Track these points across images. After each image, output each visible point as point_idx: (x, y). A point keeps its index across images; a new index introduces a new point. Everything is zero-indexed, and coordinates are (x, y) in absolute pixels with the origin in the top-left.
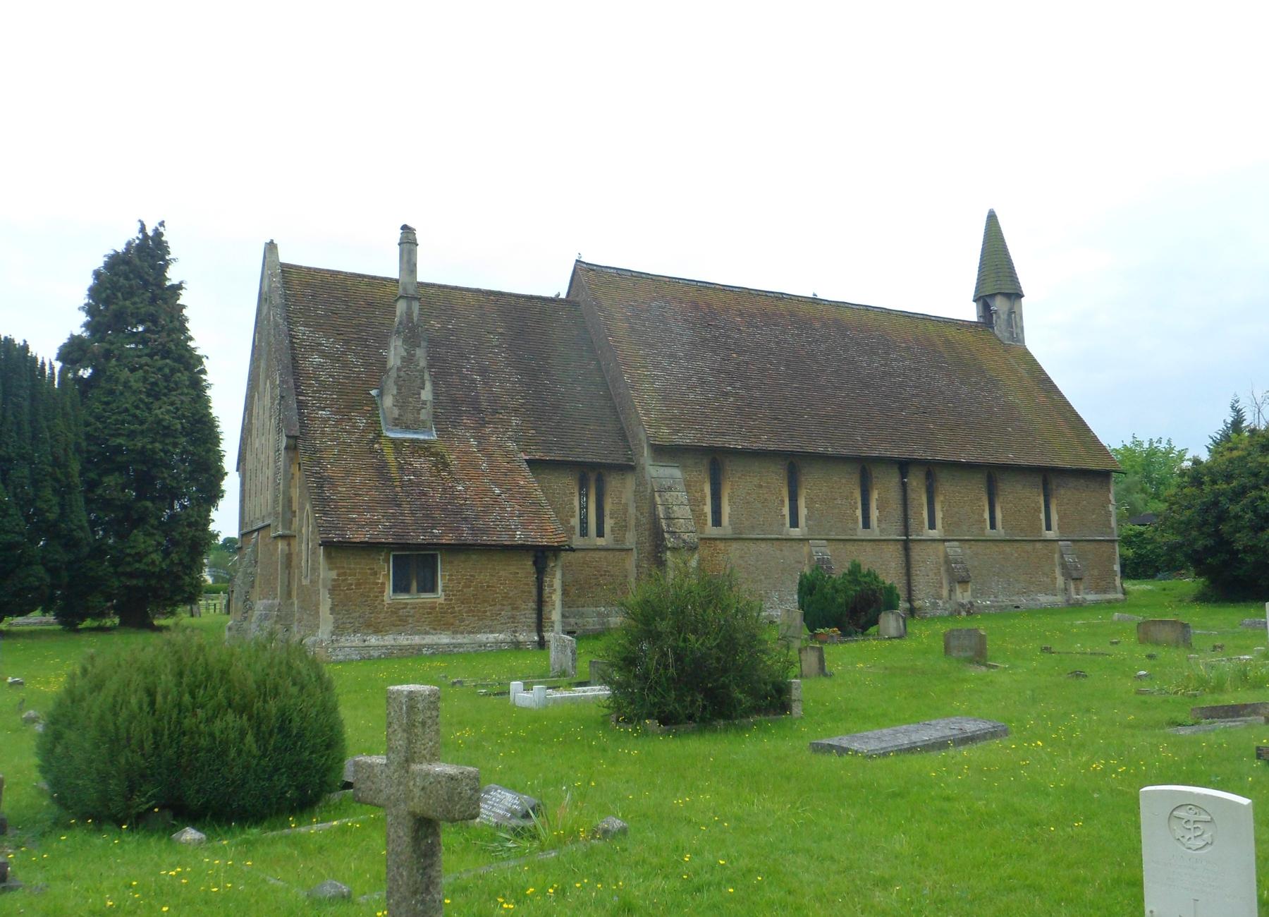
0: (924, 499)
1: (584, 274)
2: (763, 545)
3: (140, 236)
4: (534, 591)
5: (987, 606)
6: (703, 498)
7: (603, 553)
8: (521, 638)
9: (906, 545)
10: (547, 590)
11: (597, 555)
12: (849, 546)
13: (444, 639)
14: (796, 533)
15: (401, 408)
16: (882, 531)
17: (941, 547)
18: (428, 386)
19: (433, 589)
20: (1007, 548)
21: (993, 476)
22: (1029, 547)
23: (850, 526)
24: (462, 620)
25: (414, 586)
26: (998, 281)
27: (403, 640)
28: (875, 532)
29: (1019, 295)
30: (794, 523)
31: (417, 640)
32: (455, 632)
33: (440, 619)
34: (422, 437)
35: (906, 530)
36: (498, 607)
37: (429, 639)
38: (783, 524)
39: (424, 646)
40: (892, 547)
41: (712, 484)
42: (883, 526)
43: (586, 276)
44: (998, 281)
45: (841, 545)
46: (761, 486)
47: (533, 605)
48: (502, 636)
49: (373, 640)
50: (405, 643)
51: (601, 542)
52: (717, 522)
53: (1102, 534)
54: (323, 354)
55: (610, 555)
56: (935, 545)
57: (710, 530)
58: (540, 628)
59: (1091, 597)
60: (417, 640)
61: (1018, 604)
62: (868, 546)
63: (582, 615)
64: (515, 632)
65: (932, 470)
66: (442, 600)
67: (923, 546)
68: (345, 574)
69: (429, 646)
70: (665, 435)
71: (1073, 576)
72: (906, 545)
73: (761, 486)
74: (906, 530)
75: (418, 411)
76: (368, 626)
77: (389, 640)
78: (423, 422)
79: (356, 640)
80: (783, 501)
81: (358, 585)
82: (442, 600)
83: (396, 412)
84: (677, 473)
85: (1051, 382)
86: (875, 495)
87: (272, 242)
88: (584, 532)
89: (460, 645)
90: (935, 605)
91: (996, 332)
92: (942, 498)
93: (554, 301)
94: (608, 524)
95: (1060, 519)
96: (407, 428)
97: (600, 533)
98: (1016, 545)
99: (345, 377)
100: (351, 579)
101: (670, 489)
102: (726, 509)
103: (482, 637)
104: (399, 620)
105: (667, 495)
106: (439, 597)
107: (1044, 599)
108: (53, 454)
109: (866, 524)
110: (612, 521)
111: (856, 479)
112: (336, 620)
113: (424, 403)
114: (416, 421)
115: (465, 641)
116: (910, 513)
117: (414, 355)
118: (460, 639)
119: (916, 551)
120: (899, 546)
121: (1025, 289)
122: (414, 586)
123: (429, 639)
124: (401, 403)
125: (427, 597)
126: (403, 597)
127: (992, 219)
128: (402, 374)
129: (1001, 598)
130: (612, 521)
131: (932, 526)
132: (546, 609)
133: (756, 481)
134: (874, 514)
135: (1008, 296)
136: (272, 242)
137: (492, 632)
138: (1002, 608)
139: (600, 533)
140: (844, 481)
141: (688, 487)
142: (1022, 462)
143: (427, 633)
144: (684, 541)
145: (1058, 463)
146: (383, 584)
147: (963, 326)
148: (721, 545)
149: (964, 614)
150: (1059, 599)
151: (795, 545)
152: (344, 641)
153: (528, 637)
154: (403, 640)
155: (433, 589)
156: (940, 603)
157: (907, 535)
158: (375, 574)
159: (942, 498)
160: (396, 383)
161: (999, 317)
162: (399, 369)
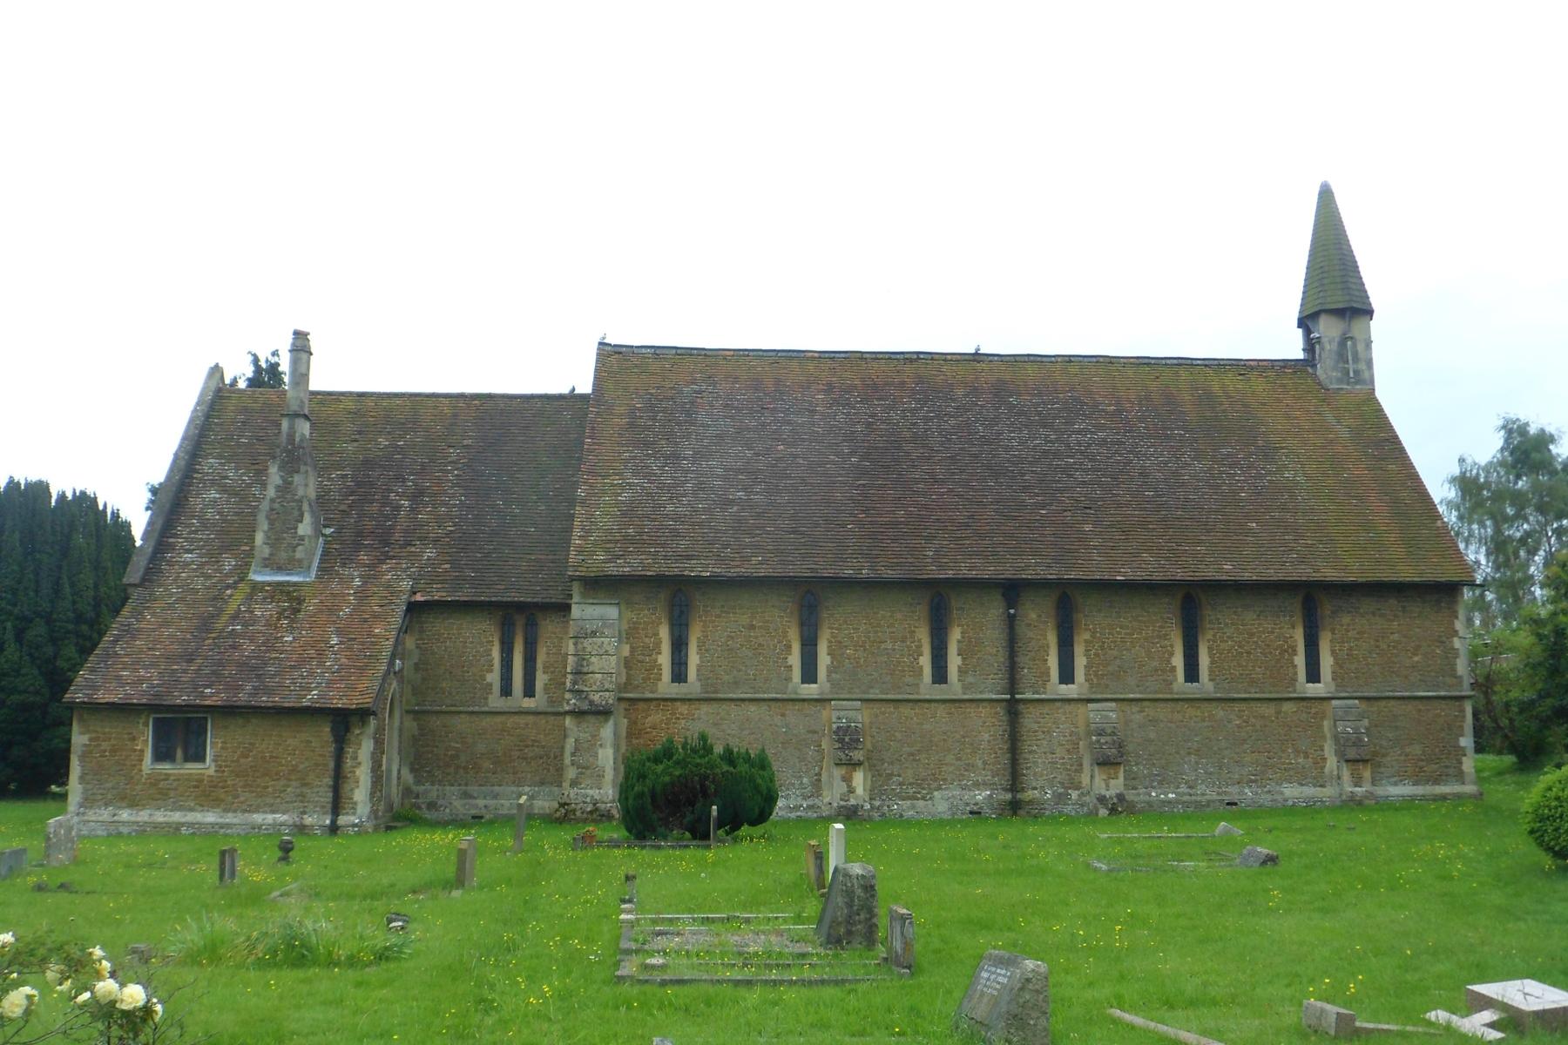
0: (1052, 639)
1: (612, 358)
2: (753, 708)
3: (252, 368)
4: (332, 765)
5: (1170, 802)
6: (658, 644)
7: (531, 718)
8: (308, 820)
9: (1013, 709)
10: (349, 762)
11: (522, 720)
12: (906, 710)
13: (210, 817)
14: (811, 690)
15: (272, 546)
16: (966, 688)
17: (1081, 709)
18: (307, 518)
19: (200, 758)
20: (1219, 712)
21: (1192, 601)
22: (1268, 710)
23: (908, 679)
24: (237, 797)
25: (179, 753)
26: (1336, 295)
27: (160, 817)
28: (955, 685)
29: (1368, 313)
30: (809, 675)
31: (177, 817)
32: (226, 810)
33: (207, 794)
34: (294, 579)
35: (1013, 684)
36: (282, 782)
37: (191, 817)
38: (789, 679)
39: (183, 824)
40: (984, 711)
41: (672, 626)
42: (970, 679)
43: (615, 361)
44: (1336, 295)
45: (891, 708)
46: (752, 627)
47: (328, 781)
48: (285, 817)
49: (125, 815)
50: (161, 820)
51: (529, 703)
52: (679, 675)
53: (1437, 687)
54: (224, 489)
55: (542, 720)
56: (1068, 707)
57: (666, 686)
58: (336, 808)
59: (1406, 790)
60: (177, 817)
61: (1235, 799)
62: (941, 710)
63: (495, 797)
64: (304, 813)
65: (1067, 600)
66: (211, 772)
67: (1046, 709)
68: (97, 739)
69: (190, 825)
70: (600, 562)
71: (1358, 758)
72: (1013, 709)
73: (752, 627)
74: (1013, 684)
75: (294, 548)
76: (123, 799)
77: (144, 816)
78: (300, 561)
79: (105, 814)
80: (789, 647)
81: (114, 751)
82: (211, 772)
83: (267, 551)
84: (612, 612)
85: (1399, 443)
86: (955, 635)
87: (217, 365)
88: (506, 691)
89: (228, 826)
90: (1061, 798)
91: (1319, 372)
92: (1087, 636)
93: (572, 398)
94: (541, 679)
95: (1338, 663)
96: (280, 569)
97: (529, 691)
98: (1237, 706)
99: (237, 514)
100: (105, 745)
101: (593, 634)
102: (694, 659)
103: (258, 818)
104: (160, 793)
105: (586, 643)
106: (207, 768)
107: (1291, 791)
108: (74, 611)
109: (940, 675)
110: (546, 677)
111: (922, 611)
112: (85, 791)
113: (302, 538)
114: (292, 560)
115: (235, 821)
116: (1022, 660)
117: (291, 483)
118: (230, 818)
119: (1031, 720)
120: (1000, 710)
121: (1374, 306)
122: (179, 753)
123: (191, 817)
124: (274, 541)
125: (193, 768)
126: (166, 767)
127: (1326, 197)
128: (276, 506)
129: (1200, 789)
130: (546, 677)
131: (1067, 676)
132: (346, 787)
133: (745, 620)
134: (954, 661)
135: (1340, 313)
136: (217, 365)
137: (273, 812)
138: (1199, 806)
139: (529, 691)
140: (899, 616)
141: (630, 634)
142: (1246, 576)
143: (191, 810)
144: (591, 703)
145: (1330, 574)
146: (142, 751)
147: (1265, 369)
148: (683, 709)
149: (1103, 812)
150: (1329, 792)
151: (810, 709)
152: (91, 815)
153: (317, 819)
154: (160, 817)
155: (200, 758)
156: (1074, 795)
157: (1012, 694)
158: (134, 739)
159: (1209, 635)
160: (267, 517)
161: (1322, 349)
162: (273, 501)
